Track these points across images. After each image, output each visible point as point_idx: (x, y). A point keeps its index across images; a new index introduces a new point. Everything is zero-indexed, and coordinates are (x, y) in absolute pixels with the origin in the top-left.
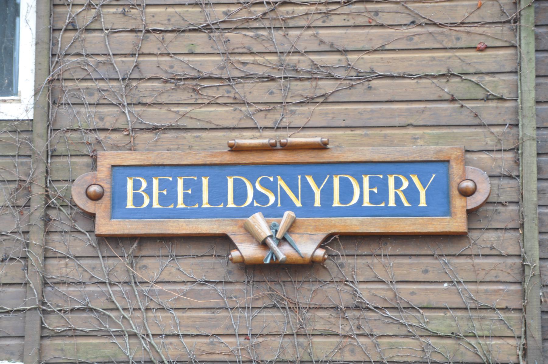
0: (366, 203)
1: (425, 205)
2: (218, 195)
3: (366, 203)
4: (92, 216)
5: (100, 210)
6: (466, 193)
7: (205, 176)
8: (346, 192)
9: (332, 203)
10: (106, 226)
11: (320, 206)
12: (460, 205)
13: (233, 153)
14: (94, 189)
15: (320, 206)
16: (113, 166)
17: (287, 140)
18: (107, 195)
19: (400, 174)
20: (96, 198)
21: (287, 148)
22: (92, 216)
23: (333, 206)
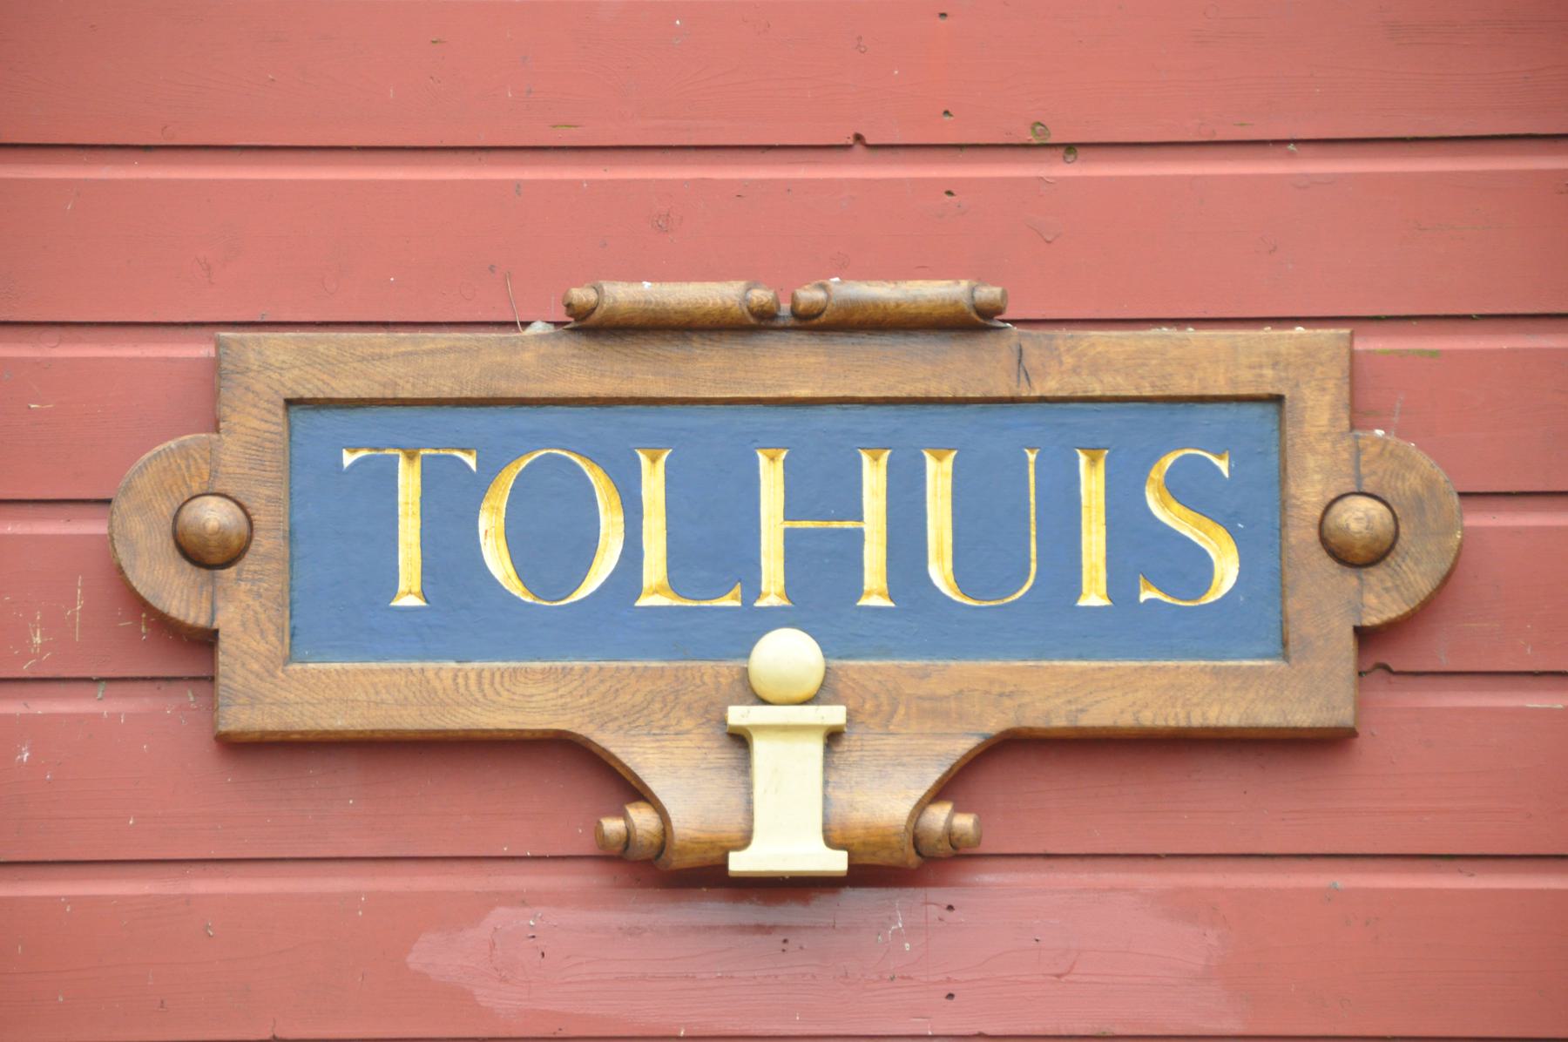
0: (655, 591)
1: (415, 601)
2: (554, 539)
3: (655, 591)
4: (205, 641)
5: (242, 612)
6: (1355, 557)
7: (940, 448)
8: (554, 539)
9: (1077, 592)
10: (281, 684)
11: (1106, 602)
12: (1332, 607)
13: (583, 340)
14: (214, 515)
15: (1106, 602)
16: (290, 403)
17: (599, 290)
18: (266, 542)
19: (593, 459)
20: (206, 557)
21: (810, 323)
22: (205, 641)
23: (1082, 602)
